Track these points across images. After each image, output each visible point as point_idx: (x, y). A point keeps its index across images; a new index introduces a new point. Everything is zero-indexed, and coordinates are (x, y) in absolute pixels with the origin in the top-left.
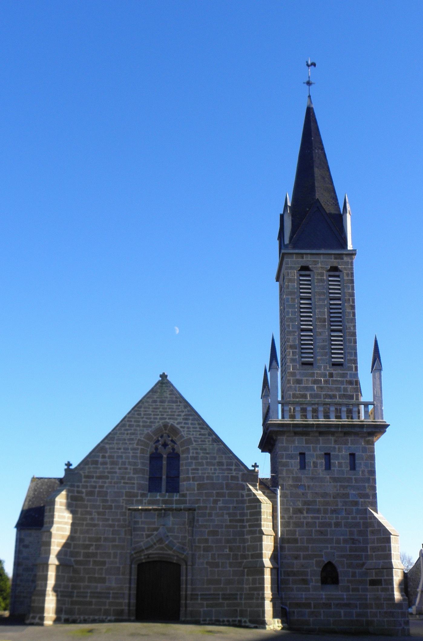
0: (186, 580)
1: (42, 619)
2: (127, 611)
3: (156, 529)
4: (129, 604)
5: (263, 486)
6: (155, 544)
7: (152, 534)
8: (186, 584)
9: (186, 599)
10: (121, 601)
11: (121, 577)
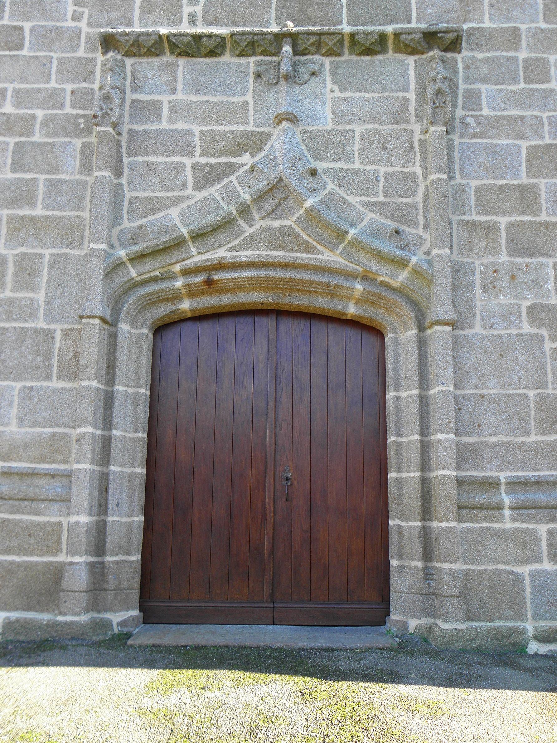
0: (424, 402)
1: (330, 64)
2: (78, 579)
3: (255, 143)
4: (98, 540)
5: (344, 318)
6: (244, 211)
7: (231, 168)
8: (424, 429)
9: (427, 512)
10: (50, 517)
11: (55, 384)
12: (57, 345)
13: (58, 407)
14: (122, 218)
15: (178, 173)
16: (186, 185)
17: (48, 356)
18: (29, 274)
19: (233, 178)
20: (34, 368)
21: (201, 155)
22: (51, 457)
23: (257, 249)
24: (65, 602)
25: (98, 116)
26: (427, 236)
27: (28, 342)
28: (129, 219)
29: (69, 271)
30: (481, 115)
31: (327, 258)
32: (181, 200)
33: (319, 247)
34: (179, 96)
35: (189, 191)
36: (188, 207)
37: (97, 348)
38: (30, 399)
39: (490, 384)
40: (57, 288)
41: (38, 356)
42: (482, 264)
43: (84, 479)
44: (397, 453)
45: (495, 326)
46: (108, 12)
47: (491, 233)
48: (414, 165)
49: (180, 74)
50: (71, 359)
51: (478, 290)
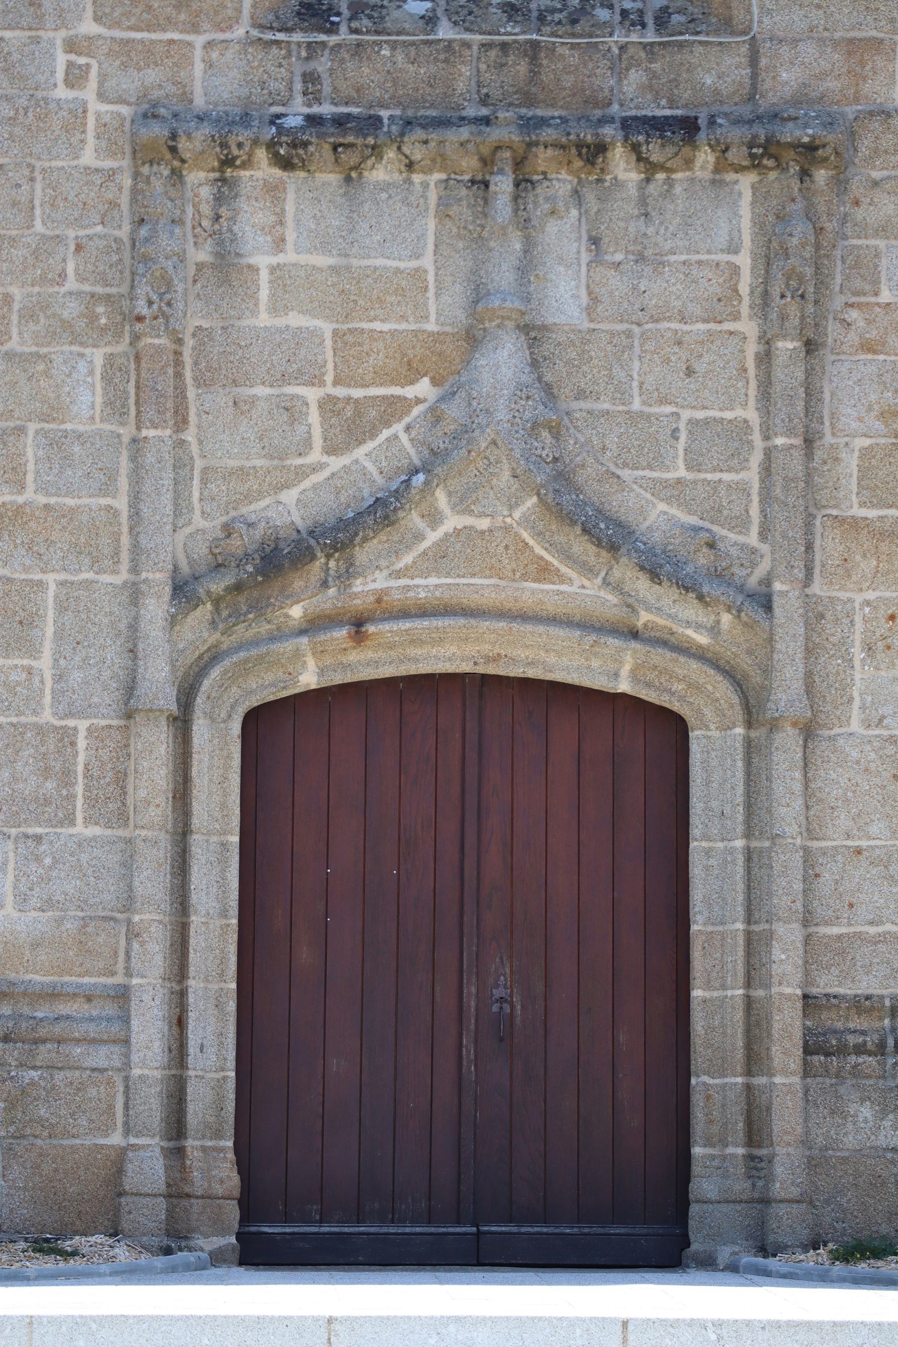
12: (81, 759)
13: (90, 872)
14: (191, 510)
15: (293, 421)
16: (310, 444)
17: (67, 777)
18: (21, 622)
19: (398, 428)
20: (42, 801)
21: (336, 382)
22: (81, 964)
23: (448, 575)
24: (130, 1213)
25: (145, 318)
26: (765, 548)
27: (27, 753)
28: (203, 513)
29: (95, 615)
30: (878, 304)
31: (578, 591)
32: (302, 473)
33: (564, 569)
34: (289, 256)
35: (315, 456)
36: (315, 487)
37: (164, 768)
38: (38, 859)
39: (874, 829)
40: (74, 649)
41: (46, 779)
42: (868, 603)
43: (153, 1004)
44: (705, 954)
45: (885, 721)
46: (139, 70)
47: (887, 542)
48: (745, 405)
49: (290, 208)
50: (108, 784)
51: (858, 654)
